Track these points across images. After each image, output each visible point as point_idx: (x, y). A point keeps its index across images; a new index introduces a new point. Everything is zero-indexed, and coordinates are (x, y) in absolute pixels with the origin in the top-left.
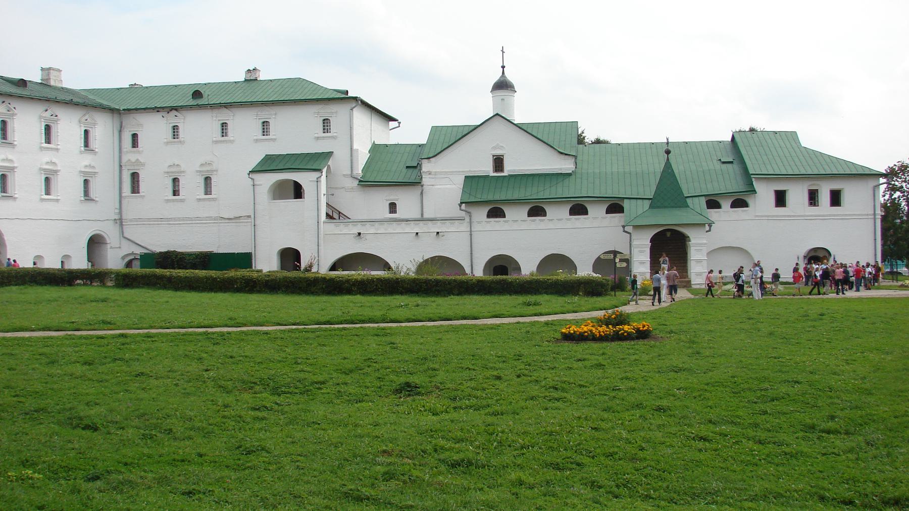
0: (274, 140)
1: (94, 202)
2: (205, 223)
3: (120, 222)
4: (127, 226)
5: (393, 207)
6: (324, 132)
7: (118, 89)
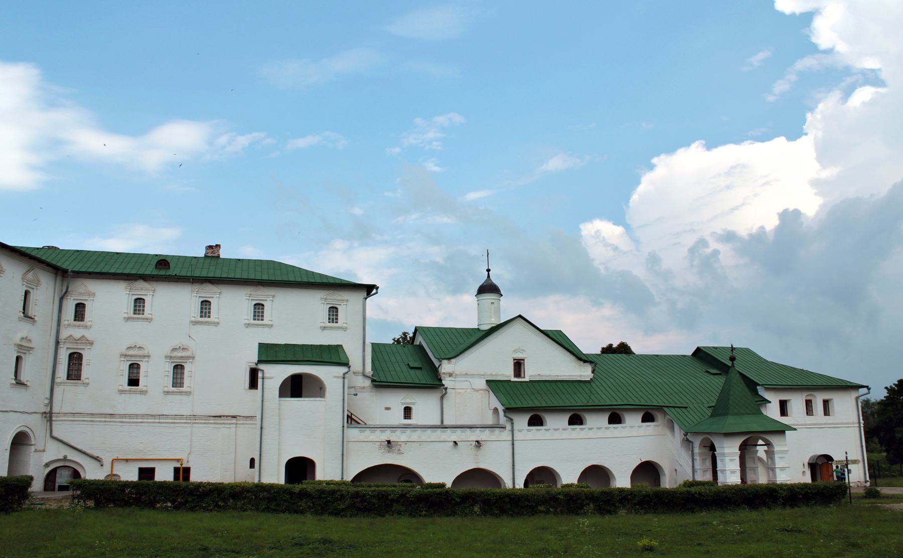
0: (217, 324)
1: (23, 387)
2: (221, 424)
3: (49, 416)
4: (58, 423)
5: (408, 412)
6: (329, 322)
7: (118, 253)
